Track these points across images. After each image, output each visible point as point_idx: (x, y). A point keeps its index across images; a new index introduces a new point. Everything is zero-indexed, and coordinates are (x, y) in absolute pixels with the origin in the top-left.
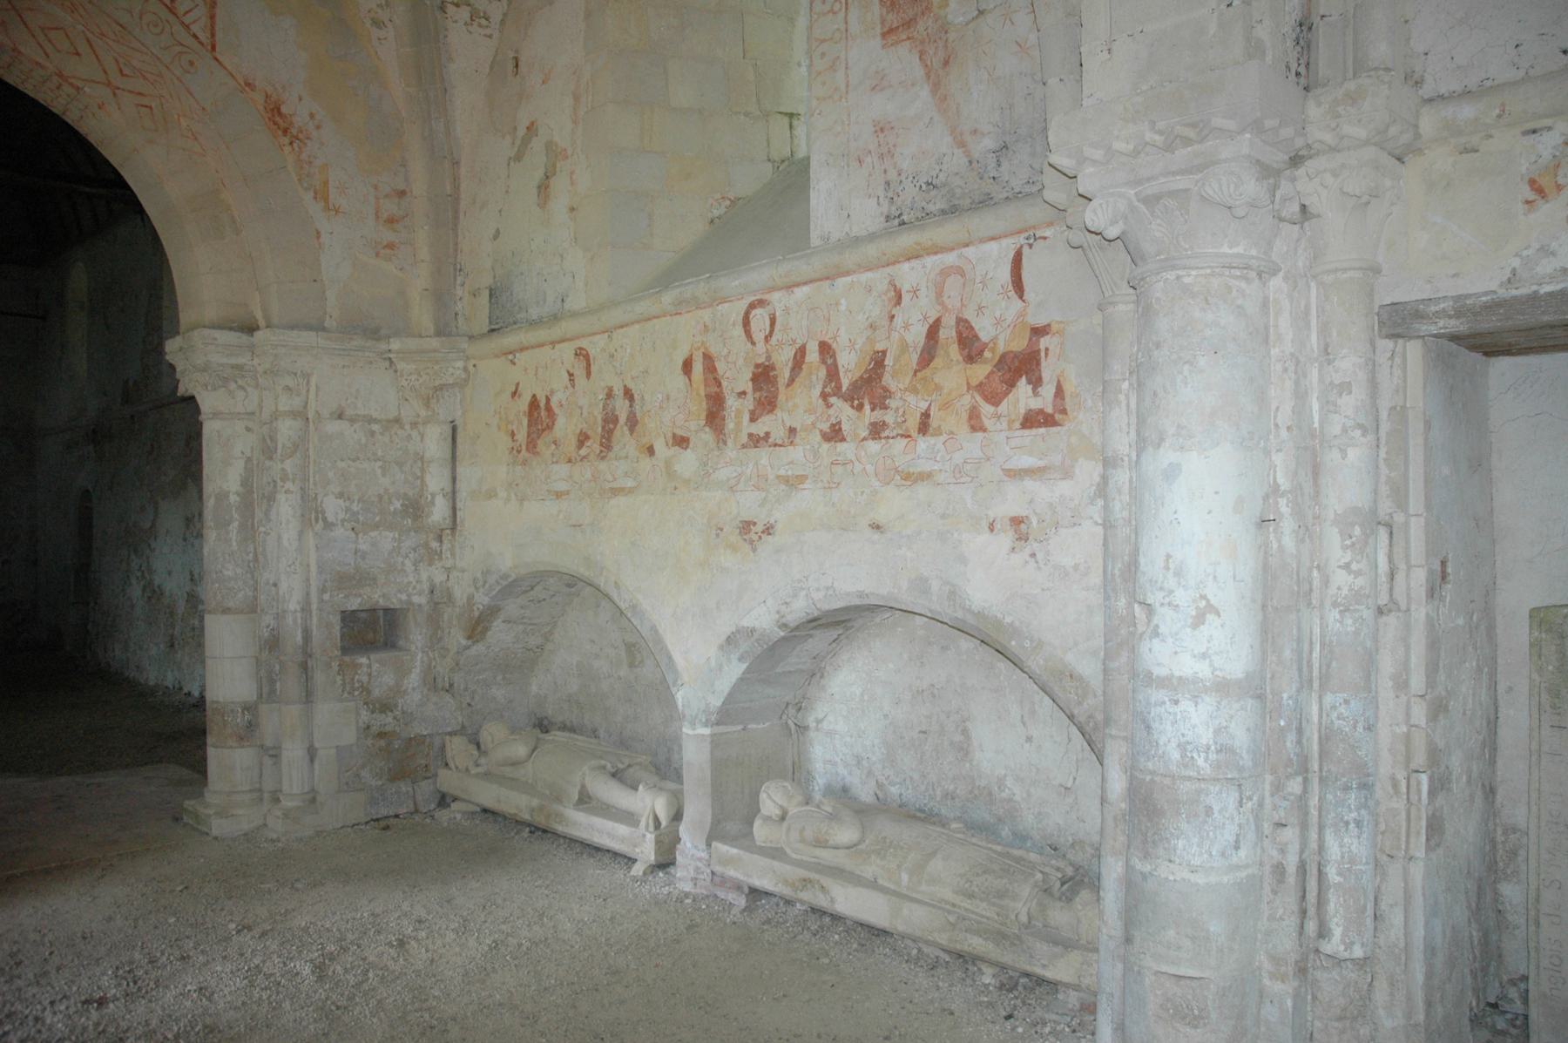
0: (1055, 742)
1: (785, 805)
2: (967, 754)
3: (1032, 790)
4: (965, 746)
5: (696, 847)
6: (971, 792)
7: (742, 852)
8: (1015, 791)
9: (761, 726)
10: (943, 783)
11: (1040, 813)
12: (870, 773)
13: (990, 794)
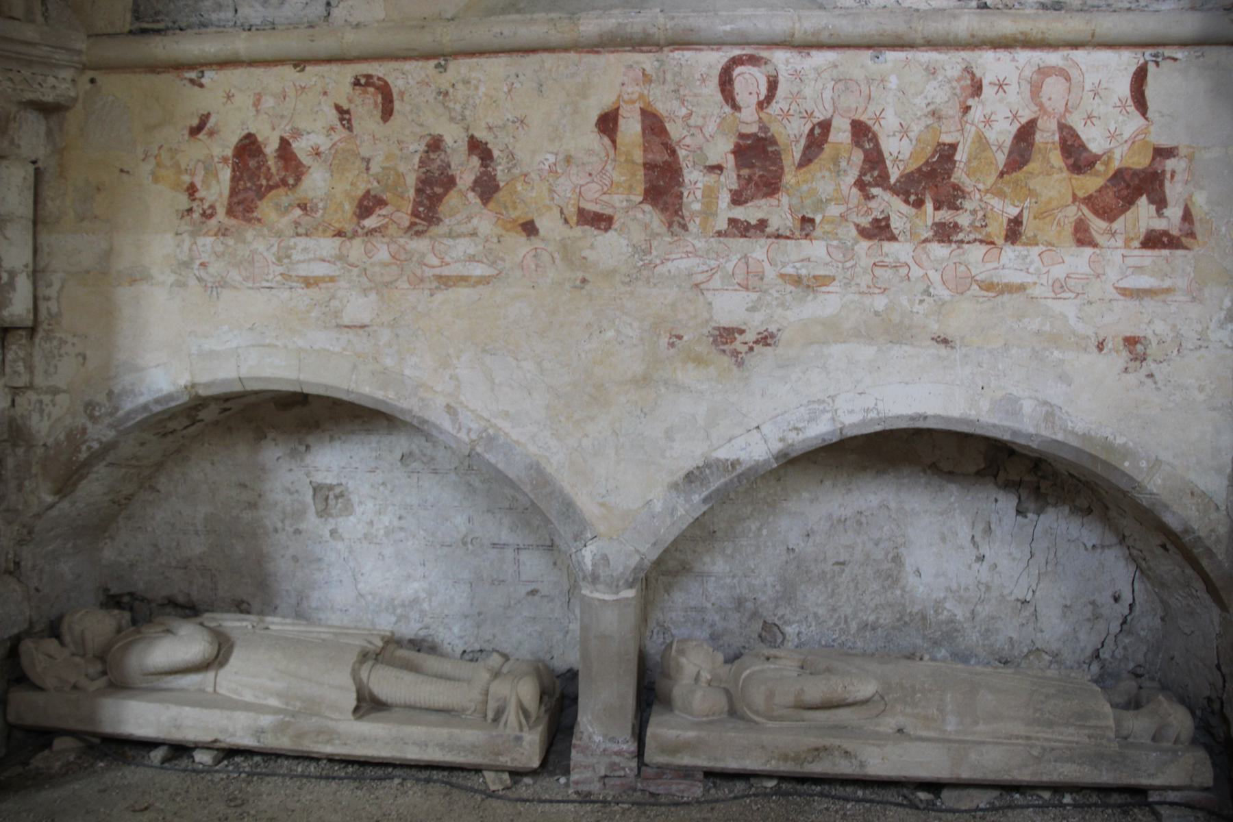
0: (1014, 559)
2: (896, 581)
3: (979, 608)
4: (895, 573)
6: (898, 620)
11: (987, 630)
12: (755, 614)
13: (924, 618)
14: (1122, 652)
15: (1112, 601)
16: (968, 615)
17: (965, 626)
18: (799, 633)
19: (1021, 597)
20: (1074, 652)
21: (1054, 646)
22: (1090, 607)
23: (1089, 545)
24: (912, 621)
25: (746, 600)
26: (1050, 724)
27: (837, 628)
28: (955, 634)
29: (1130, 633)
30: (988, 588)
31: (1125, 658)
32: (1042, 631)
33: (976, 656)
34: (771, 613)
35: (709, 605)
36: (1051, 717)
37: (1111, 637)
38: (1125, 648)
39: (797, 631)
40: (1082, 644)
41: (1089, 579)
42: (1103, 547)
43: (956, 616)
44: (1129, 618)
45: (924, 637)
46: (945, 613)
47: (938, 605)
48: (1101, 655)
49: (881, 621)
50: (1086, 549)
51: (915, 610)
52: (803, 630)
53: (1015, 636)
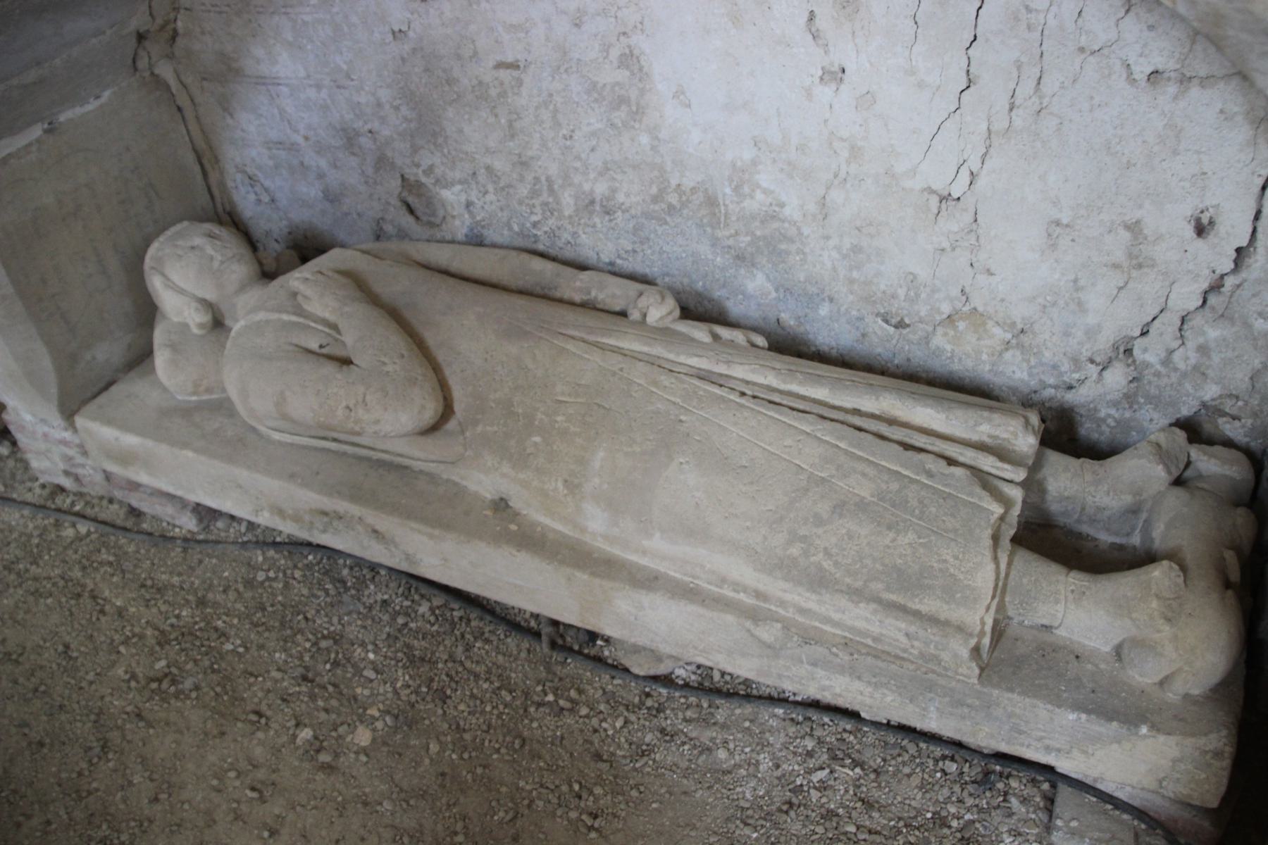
0: (921, 85)
1: (210, 296)
2: (638, 113)
3: (836, 196)
4: (633, 94)
5: (43, 421)
6: (656, 199)
7: (149, 443)
8: (784, 198)
9: (92, 106)
10: (577, 179)
11: (856, 249)
12: (382, 162)
13: (711, 202)
14: (1194, 358)
15: (1189, 231)
16: (812, 207)
17: (806, 231)
18: (469, 205)
19: (939, 185)
20: (1067, 334)
21: (1019, 313)
22: (1125, 235)
23: (1142, 69)
24: (684, 205)
25: (358, 134)
26: (819, 582)
27: (536, 202)
28: (783, 247)
29: (1224, 316)
30: (855, 152)
31: (1199, 372)
32: (989, 273)
33: (831, 300)
34: (408, 161)
35: (300, 140)
36: (827, 564)
37: (1172, 319)
38: (1203, 350)
39: (463, 198)
40: (1091, 320)
41: (1129, 165)
42: (1185, 81)
43: (782, 205)
44: (1230, 282)
45: (715, 242)
46: (759, 196)
47: (742, 179)
48: (1136, 352)
49: (621, 197)
50: (1131, 80)
51: (688, 183)
52: (474, 199)
53: (923, 274)
